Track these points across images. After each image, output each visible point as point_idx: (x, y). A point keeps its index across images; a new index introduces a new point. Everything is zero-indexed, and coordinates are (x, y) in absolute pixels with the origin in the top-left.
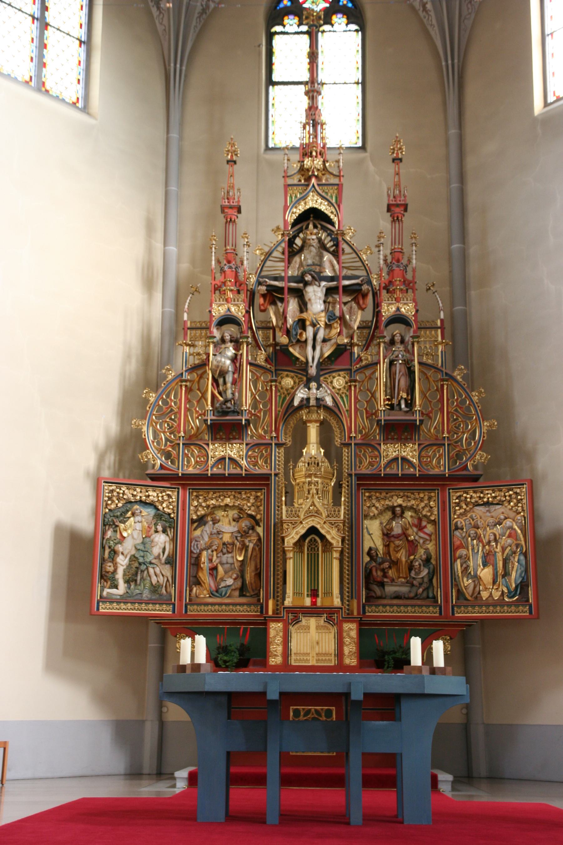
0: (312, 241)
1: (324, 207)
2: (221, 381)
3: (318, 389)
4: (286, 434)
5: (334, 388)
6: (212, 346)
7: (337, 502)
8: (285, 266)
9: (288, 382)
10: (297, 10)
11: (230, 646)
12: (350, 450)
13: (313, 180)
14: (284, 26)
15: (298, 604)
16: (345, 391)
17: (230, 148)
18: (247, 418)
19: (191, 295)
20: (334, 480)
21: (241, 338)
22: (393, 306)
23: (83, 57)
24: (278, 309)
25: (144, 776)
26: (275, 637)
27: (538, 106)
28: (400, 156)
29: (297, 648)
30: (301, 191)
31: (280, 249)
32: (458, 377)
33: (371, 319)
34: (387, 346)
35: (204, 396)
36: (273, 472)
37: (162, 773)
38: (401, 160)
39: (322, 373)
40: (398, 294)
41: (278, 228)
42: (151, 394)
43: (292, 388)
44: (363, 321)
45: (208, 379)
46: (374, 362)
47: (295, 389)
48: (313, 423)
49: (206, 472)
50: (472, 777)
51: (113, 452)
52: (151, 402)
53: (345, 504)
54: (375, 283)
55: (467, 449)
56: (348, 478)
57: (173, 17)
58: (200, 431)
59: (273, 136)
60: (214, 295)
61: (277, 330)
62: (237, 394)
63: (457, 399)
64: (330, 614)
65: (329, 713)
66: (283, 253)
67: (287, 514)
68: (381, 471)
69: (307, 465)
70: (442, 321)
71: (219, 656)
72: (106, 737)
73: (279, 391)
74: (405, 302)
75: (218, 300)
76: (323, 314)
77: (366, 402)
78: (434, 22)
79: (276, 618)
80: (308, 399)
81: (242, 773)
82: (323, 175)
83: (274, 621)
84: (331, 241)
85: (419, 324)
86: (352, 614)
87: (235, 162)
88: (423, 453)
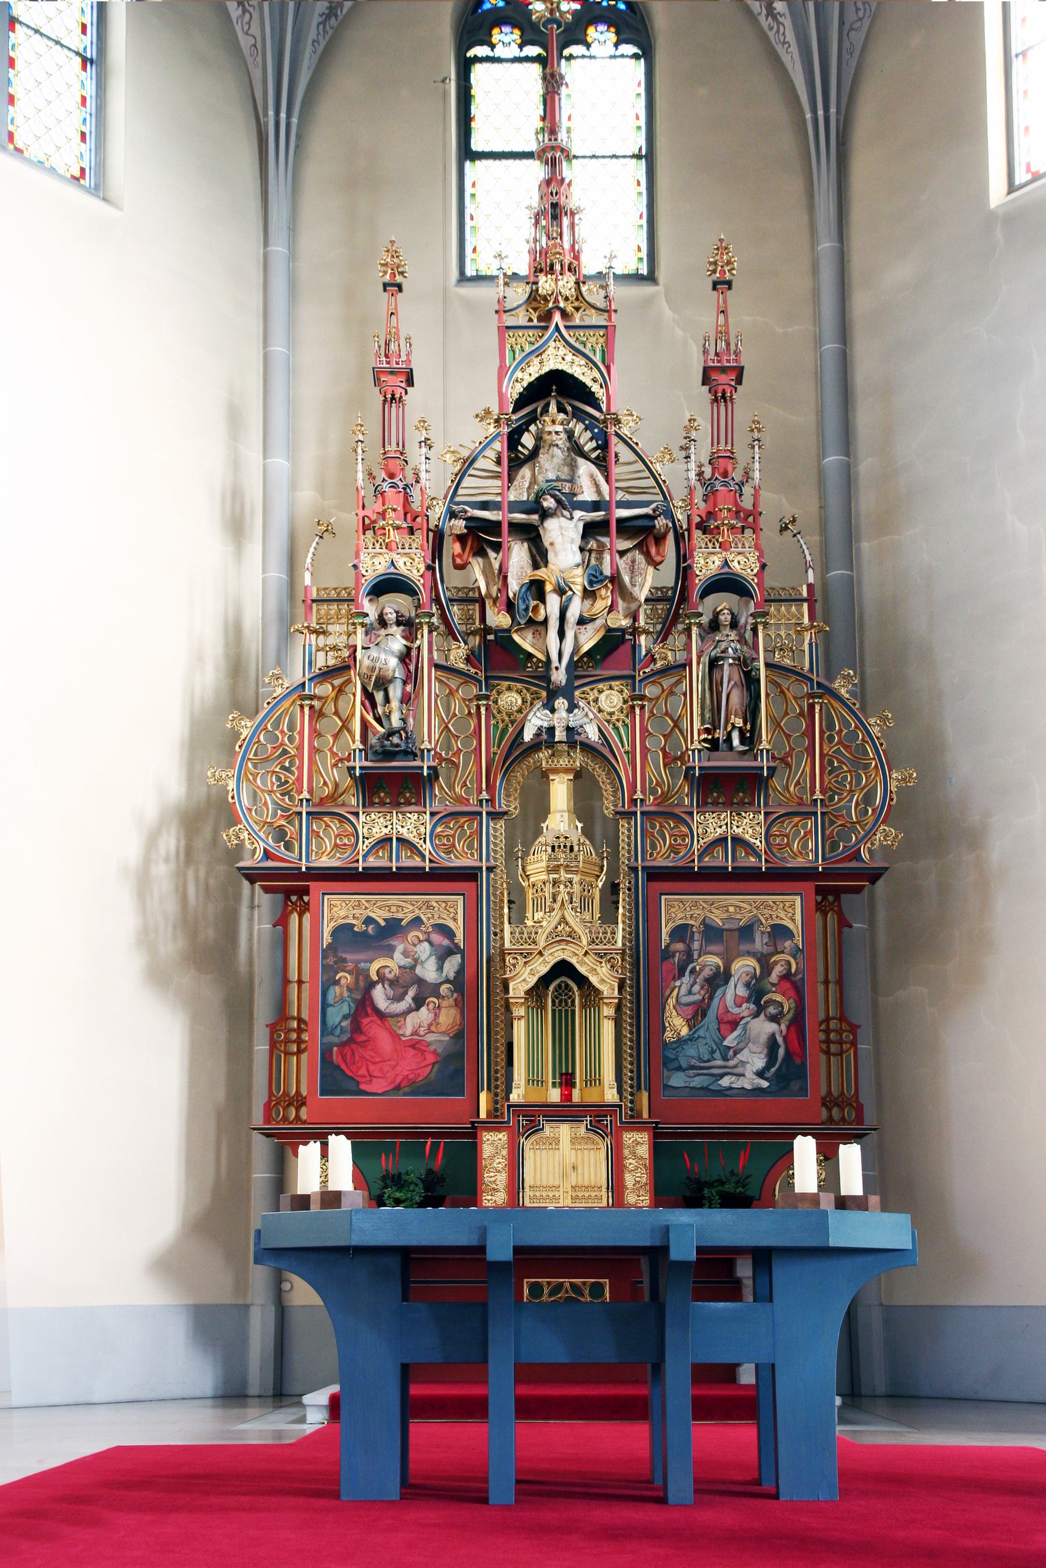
0: (554, 437)
1: (579, 370)
2: (379, 697)
3: (570, 710)
4: (508, 795)
5: (600, 711)
6: (360, 631)
7: (609, 916)
8: (503, 486)
9: (510, 699)
10: (515, 15)
11: (407, 1173)
12: (633, 823)
13: (557, 317)
14: (493, 47)
15: (535, 1098)
16: (622, 717)
17: (389, 260)
18: (432, 764)
19: (317, 539)
20: (603, 877)
21: (417, 616)
22: (715, 558)
23: (90, 91)
24: (491, 564)
25: (249, 1400)
26: (492, 1157)
27: (997, 194)
28: (728, 276)
29: (535, 1178)
30: (533, 339)
31: (491, 454)
32: (843, 691)
33: (672, 584)
34: (703, 634)
35: (346, 726)
36: (484, 865)
37: (282, 1394)
38: (729, 284)
39: (577, 683)
40: (726, 536)
41: (488, 412)
42: (243, 723)
43: (520, 711)
44: (657, 589)
45: (354, 695)
46: (677, 663)
47: (525, 712)
48: (562, 775)
49: (355, 865)
50: (860, 1396)
51: (173, 831)
52: (243, 737)
53: (624, 922)
54: (680, 515)
55: (858, 822)
56: (629, 875)
57: (271, 24)
58: (340, 790)
59: (474, 256)
60: (362, 537)
61: (488, 604)
62: (411, 720)
63: (840, 731)
64: (598, 1119)
65: (597, 1290)
66: (498, 462)
67: (514, 937)
68: (693, 861)
69: (549, 849)
70: (810, 587)
71: (386, 1191)
72: (176, 1333)
73: (494, 717)
74: (740, 550)
75: (371, 546)
76: (579, 571)
77: (664, 736)
78: (790, 37)
79: (494, 1124)
80: (551, 730)
81: (435, 1393)
82: (577, 309)
83: (490, 1130)
84: (591, 439)
85: (766, 593)
86: (640, 1116)
87: (400, 287)
88: (775, 830)
